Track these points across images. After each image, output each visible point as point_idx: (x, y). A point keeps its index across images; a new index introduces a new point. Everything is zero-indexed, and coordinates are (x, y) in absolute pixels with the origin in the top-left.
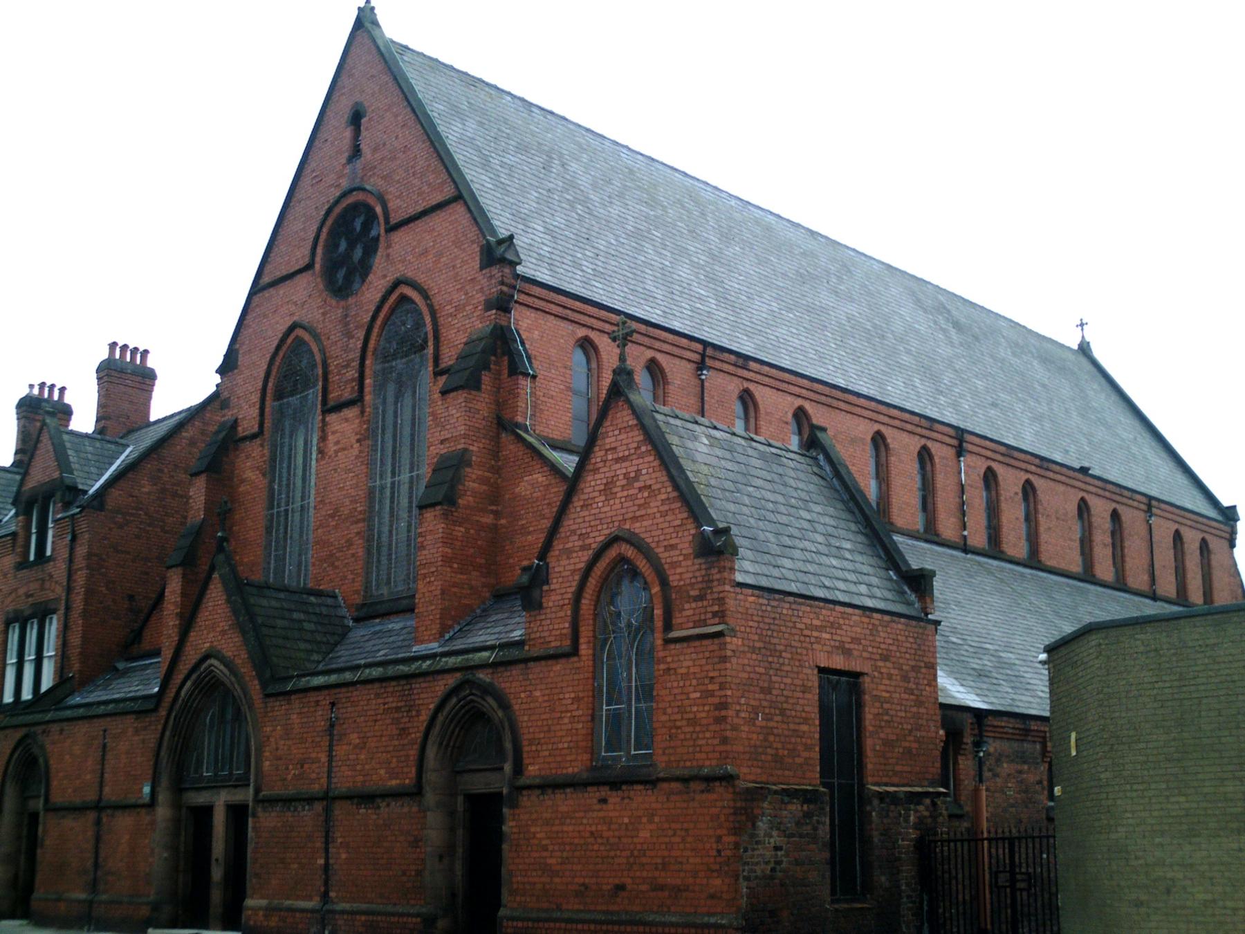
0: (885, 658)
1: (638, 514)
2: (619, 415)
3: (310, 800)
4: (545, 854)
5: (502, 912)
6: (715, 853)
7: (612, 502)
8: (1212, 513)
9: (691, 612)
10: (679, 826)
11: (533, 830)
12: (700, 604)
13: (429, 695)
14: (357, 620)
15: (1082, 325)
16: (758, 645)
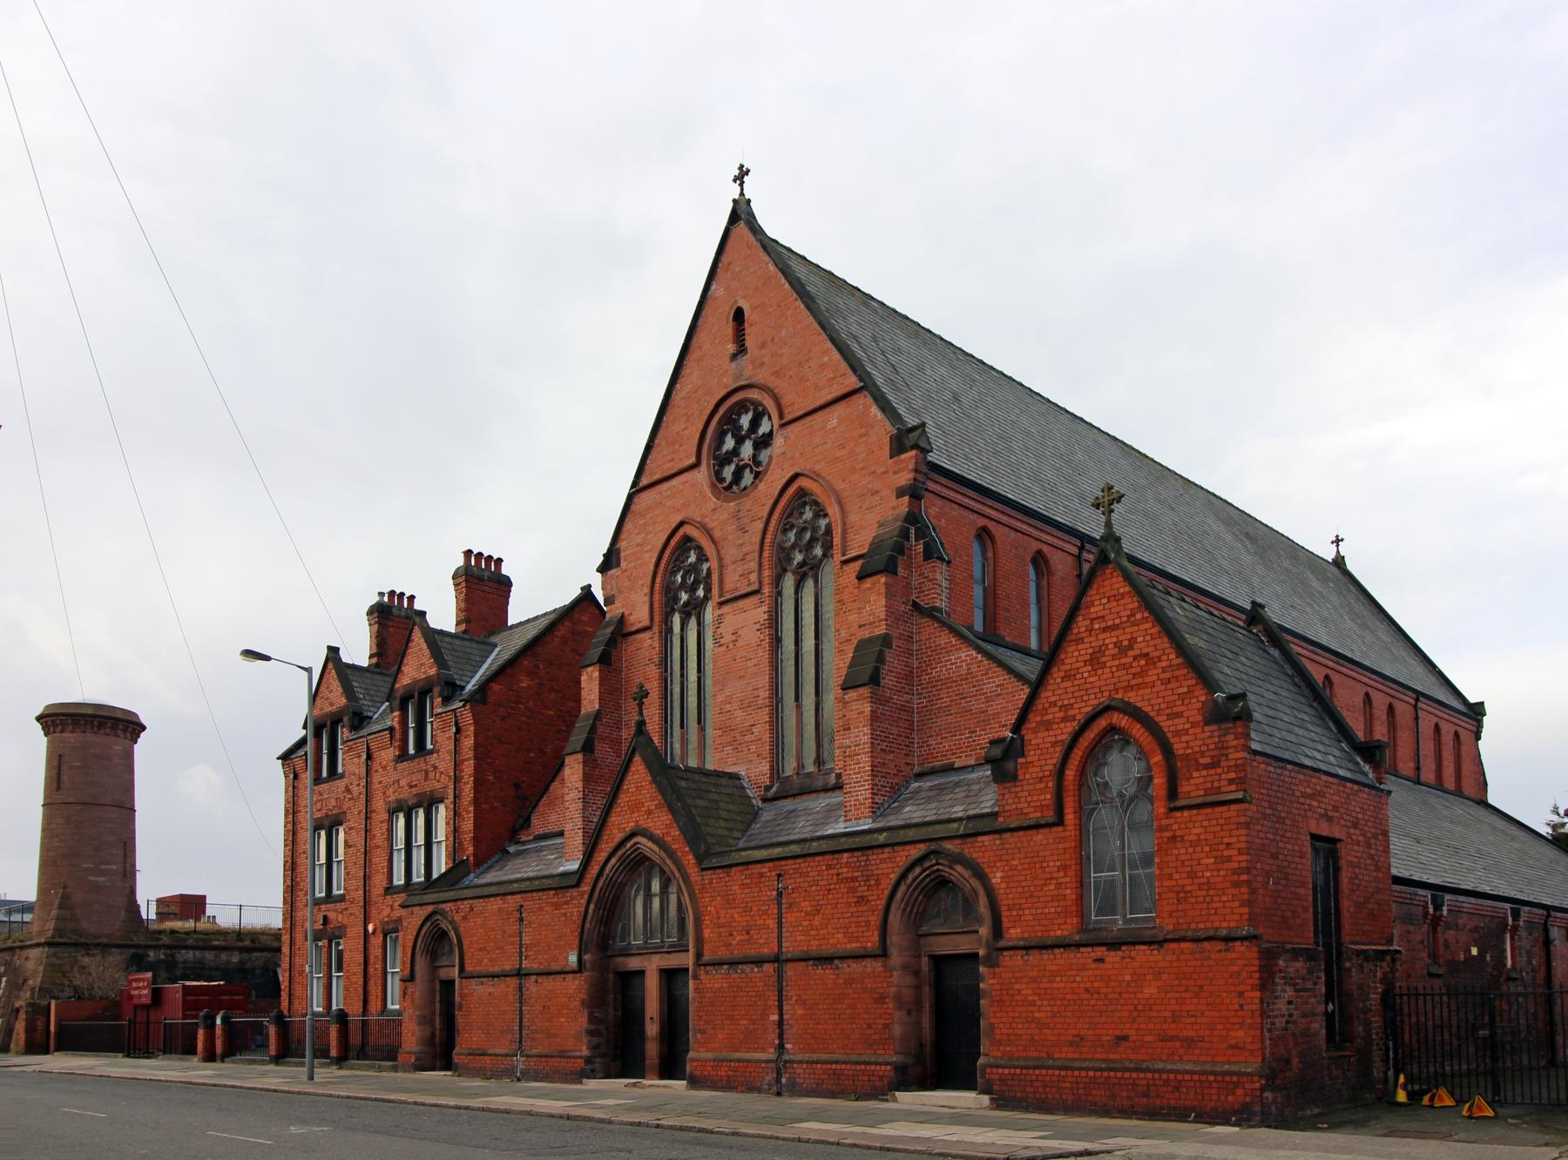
0: (1355, 825)
3: (759, 962)
5: (981, 1061)
8: (1461, 707)
12: (1212, 772)
13: (888, 866)
14: (765, 800)
15: (1338, 541)
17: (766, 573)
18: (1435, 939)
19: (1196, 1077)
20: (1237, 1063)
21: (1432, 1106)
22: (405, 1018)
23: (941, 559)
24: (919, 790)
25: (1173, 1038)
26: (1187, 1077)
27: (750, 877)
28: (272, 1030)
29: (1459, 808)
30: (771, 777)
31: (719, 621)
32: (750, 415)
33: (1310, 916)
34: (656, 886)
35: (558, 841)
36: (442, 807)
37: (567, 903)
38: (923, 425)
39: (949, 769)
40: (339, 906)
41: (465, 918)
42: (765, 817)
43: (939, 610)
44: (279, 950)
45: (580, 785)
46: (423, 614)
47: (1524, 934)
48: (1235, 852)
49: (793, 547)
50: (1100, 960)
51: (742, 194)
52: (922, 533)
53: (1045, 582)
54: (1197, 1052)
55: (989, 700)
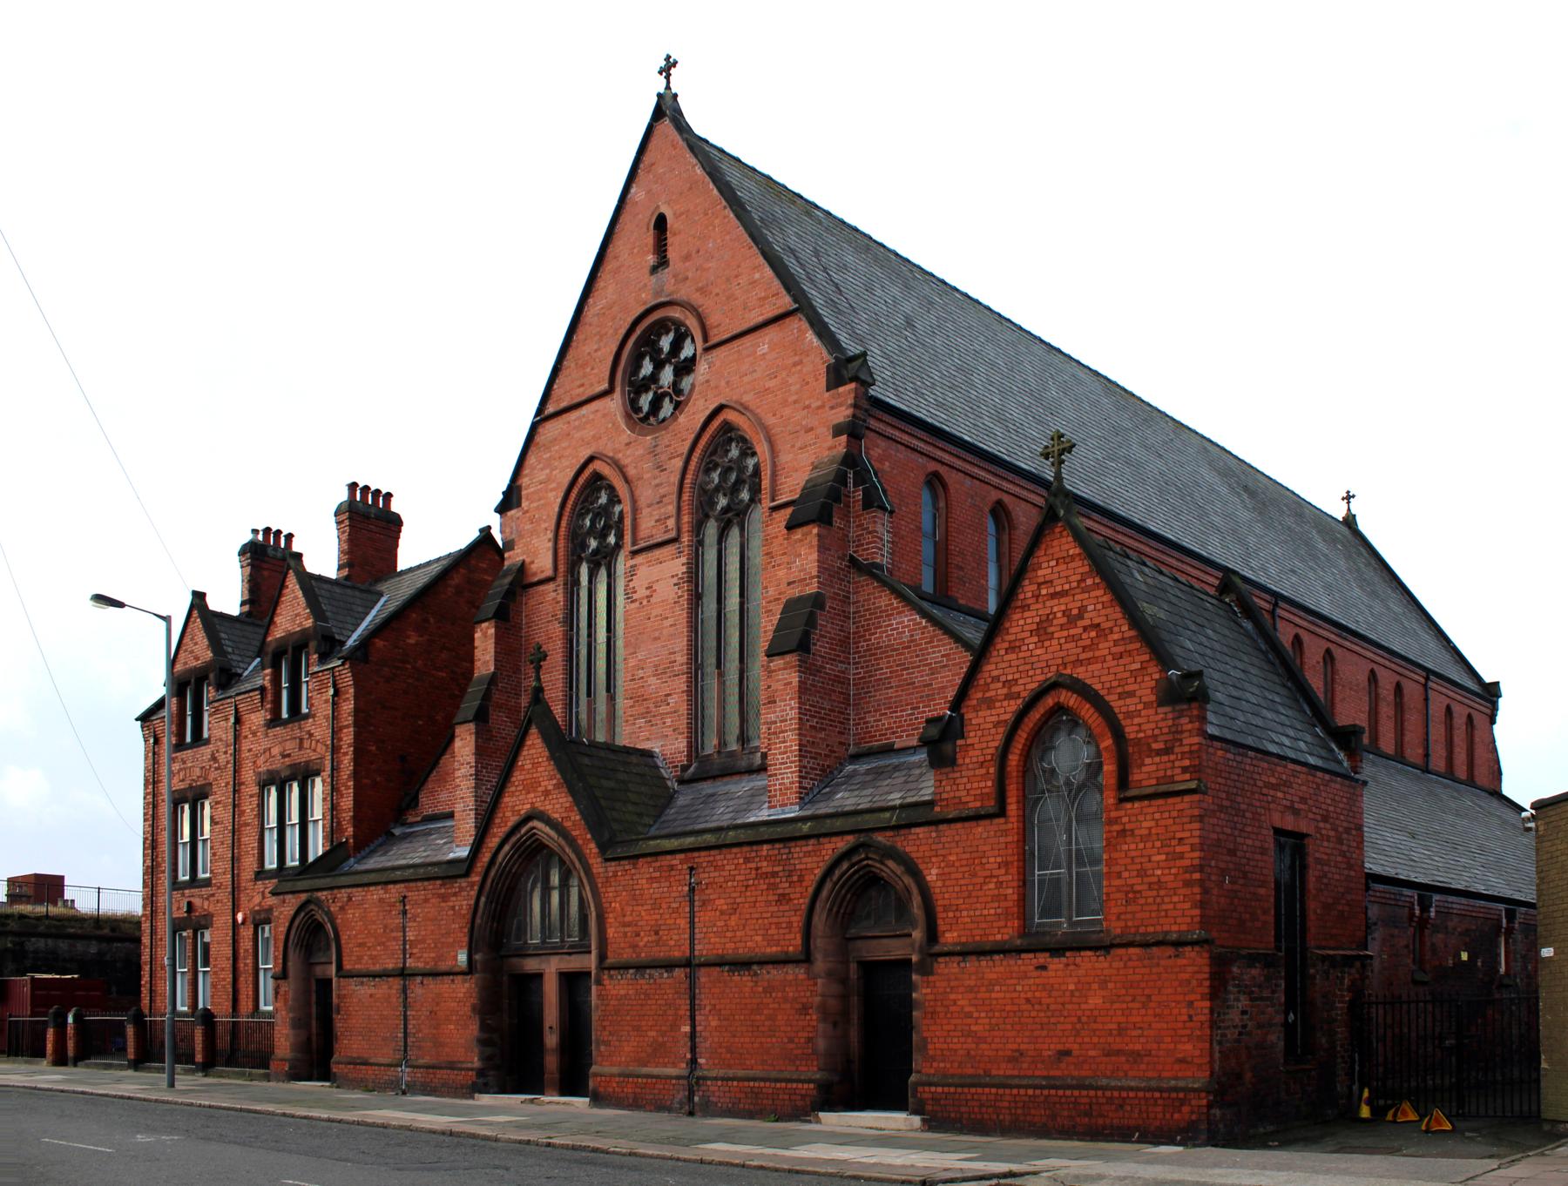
0: (1325, 819)
1: (1083, 656)
2: (1055, 543)
3: (669, 966)
4: (969, 1021)
5: (913, 1078)
6: (1185, 1018)
7: (1047, 644)
9: (1154, 768)
10: (1139, 992)
11: (953, 996)
12: (1165, 758)
13: (812, 860)
14: (681, 782)
15: (1348, 497)
16: (1225, 803)
17: (686, 519)
18: (1422, 943)
19: (1141, 1094)
20: (1183, 1078)
21: (1394, 1122)
22: (278, 1020)
23: (884, 509)
24: (854, 774)
25: (1119, 1052)
26: (1132, 1094)
27: (659, 869)
28: (130, 1030)
29: (1468, 800)
30: (689, 756)
31: (631, 573)
32: (671, 336)
33: (1271, 919)
34: (555, 879)
35: (449, 823)
36: (318, 781)
37: (455, 894)
38: (864, 354)
39: (888, 750)
40: (205, 891)
41: (342, 908)
42: (682, 800)
43: (880, 567)
44: (138, 941)
45: (472, 759)
46: (299, 556)
47: (1519, 937)
48: (1188, 848)
49: (717, 489)
50: (1044, 968)
51: (668, 87)
52: (862, 478)
53: (1006, 538)
54: (1143, 1066)
55: (933, 672)
